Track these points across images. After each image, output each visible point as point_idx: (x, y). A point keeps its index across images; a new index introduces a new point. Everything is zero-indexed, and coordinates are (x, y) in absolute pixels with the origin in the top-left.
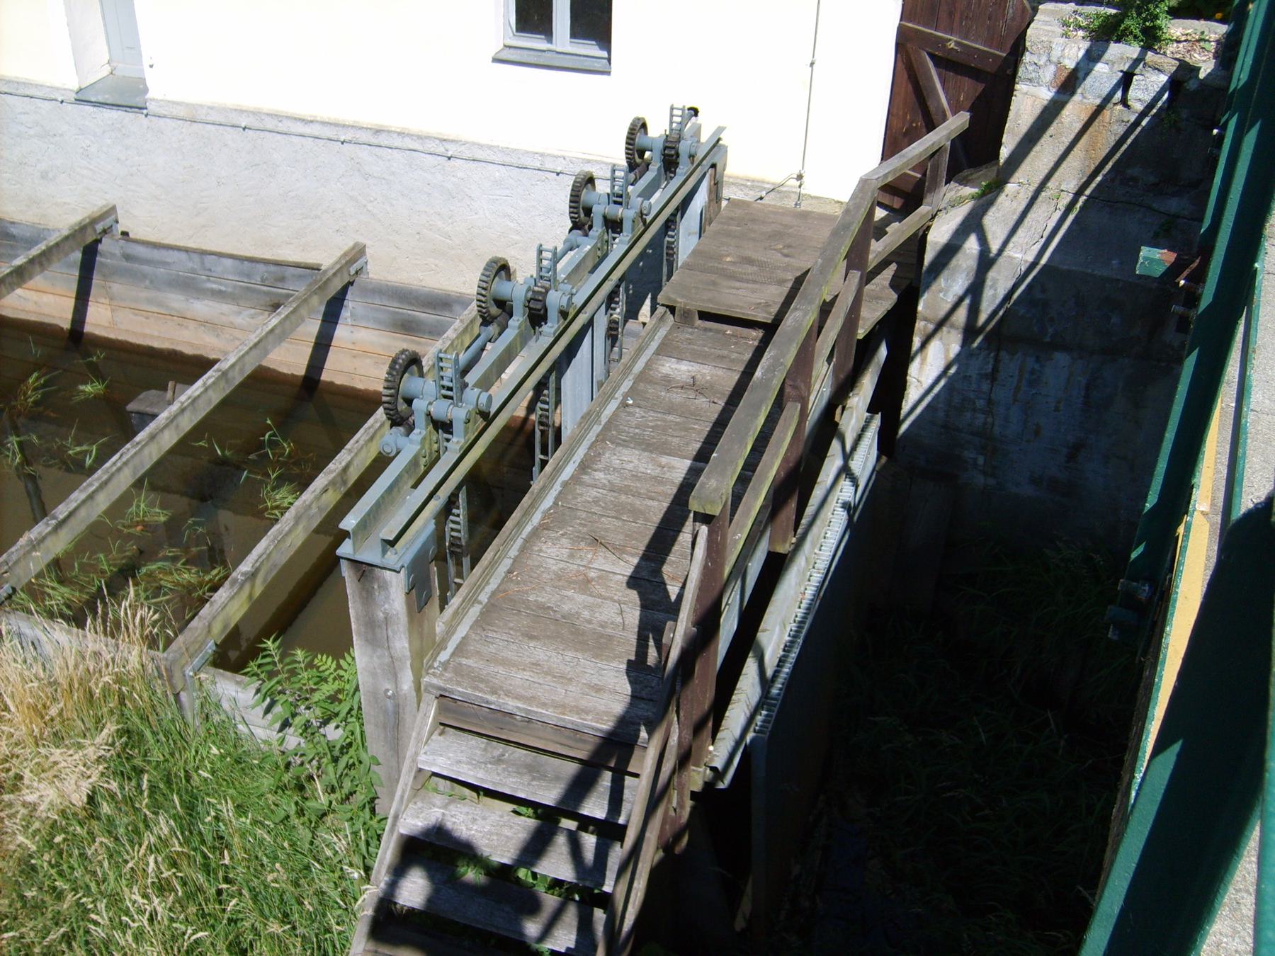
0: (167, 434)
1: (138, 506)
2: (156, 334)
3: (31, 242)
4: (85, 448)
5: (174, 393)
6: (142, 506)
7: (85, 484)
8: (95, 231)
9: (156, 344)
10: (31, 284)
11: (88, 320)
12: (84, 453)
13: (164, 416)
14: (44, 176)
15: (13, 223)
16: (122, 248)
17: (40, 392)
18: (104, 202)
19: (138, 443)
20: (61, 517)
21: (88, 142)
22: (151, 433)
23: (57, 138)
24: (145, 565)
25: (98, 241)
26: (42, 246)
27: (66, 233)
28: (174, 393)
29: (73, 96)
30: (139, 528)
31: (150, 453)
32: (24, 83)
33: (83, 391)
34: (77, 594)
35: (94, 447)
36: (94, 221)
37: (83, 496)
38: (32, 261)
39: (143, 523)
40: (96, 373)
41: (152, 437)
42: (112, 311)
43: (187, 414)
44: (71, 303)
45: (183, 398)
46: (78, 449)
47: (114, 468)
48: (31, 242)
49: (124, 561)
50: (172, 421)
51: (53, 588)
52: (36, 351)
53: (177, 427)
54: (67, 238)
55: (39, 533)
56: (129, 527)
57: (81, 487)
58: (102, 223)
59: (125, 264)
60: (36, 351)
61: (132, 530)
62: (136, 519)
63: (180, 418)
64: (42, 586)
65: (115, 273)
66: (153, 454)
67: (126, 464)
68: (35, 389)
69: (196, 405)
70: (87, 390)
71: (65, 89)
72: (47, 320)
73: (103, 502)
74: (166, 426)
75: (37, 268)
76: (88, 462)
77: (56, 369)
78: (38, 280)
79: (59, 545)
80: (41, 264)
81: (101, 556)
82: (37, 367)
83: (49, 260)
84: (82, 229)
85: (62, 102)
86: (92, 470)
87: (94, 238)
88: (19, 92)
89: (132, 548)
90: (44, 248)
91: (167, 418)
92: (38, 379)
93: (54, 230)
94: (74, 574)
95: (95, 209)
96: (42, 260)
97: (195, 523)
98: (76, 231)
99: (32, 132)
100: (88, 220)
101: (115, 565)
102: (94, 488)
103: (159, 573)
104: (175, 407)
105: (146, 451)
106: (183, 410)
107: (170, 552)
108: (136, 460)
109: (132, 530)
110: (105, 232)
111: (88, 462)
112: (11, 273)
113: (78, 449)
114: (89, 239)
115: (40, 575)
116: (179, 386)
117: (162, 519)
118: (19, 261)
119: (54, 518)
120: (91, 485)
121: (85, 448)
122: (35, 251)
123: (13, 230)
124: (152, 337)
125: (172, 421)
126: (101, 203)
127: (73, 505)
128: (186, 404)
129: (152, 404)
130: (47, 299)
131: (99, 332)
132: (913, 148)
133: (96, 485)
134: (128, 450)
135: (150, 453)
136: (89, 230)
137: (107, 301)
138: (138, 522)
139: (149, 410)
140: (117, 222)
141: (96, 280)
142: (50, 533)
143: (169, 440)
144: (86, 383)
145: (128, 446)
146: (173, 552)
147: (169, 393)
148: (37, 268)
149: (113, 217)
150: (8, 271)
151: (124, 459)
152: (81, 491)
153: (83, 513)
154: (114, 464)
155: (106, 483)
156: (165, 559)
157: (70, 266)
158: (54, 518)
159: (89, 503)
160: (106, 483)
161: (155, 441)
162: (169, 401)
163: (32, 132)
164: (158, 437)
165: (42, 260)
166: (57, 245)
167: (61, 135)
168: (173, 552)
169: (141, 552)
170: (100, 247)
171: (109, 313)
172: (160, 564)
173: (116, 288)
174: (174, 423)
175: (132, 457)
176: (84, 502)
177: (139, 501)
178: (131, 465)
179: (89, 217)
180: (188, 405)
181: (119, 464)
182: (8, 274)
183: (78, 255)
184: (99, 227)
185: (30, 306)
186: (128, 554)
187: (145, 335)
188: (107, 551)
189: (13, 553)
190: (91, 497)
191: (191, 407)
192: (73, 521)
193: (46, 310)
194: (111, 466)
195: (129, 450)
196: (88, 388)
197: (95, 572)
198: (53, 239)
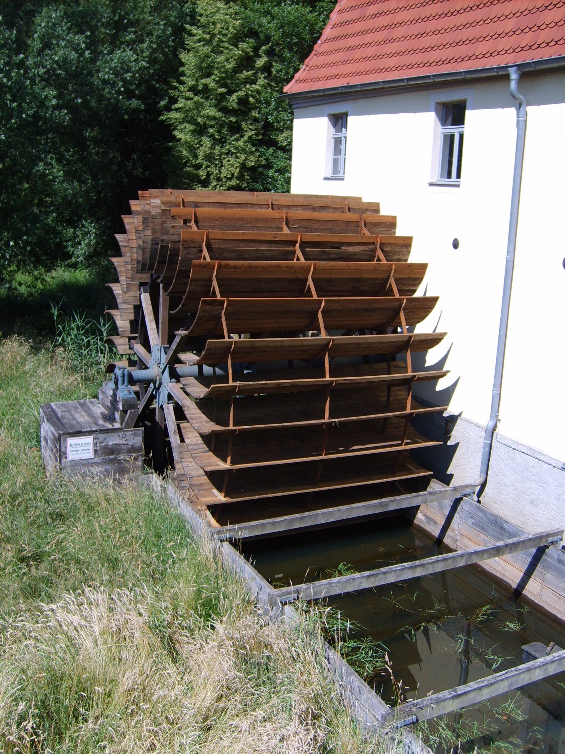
0: (538, 671)
1: (510, 705)
2: (561, 609)
3: (512, 535)
4: (495, 658)
5: (552, 649)
6: (512, 705)
7: (480, 680)
8: (547, 540)
9: (559, 616)
10: (504, 557)
11: (526, 587)
12: (494, 661)
13: (541, 660)
14: (532, 502)
15: (506, 522)
16: (559, 555)
17: (486, 617)
18: (559, 527)
19: (519, 670)
20: (459, 692)
21: (561, 492)
22: (528, 667)
23: (545, 485)
24: (498, 741)
25: (547, 547)
26: (515, 540)
27: (531, 536)
28: (552, 649)
29: (561, 465)
30: (505, 718)
31: (523, 679)
32: (538, 452)
33: (508, 626)
34: (454, 738)
35: (501, 660)
36: (548, 535)
37: (476, 686)
38: (506, 546)
39: (508, 715)
40: (520, 619)
41: (529, 670)
42: (542, 587)
43: (554, 665)
44: (521, 575)
45: (555, 655)
46: (492, 657)
47: (500, 678)
48: (512, 535)
49: (488, 733)
50: (544, 665)
51: (443, 729)
52: (494, 593)
53: (546, 669)
54: (530, 539)
55: (444, 696)
56: (500, 714)
57: (477, 681)
58: (553, 538)
59: (557, 564)
60: (494, 593)
61: (500, 717)
62: (505, 711)
63: (549, 666)
64: (439, 725)
65: (550, 567)
66: (525, 679)
67: (507, 678)
68: (484, 614)
69: (562, 661)
70: (510, 626)
71: (558, 461)
72: (505, 579)
73: (485, 694)
74: (539, 667)
75: (508, 551)
76: (494, 666)
77: (501, 608)
78: (508, 556)
79: (453, 706)
80: (511, 549)
81: (476, 723)
82: (491, 602)
83: (516, 548)
84: (540, 537)
85: (554, 467)
86: (496, 671)
87: (545, 544)
88: (534, 455)
89: (495, 727)
90: (516, 541)
91: (542, 663)
92: (488, 609)
93: (525, 533)
94: (458, 726)
95: (553, 529)
96: (512, 547)
97: (538, 731)
98: (537, 537)
99: (534, 478)
100: (545, 534)
101: (482, 732)
102: (484, 684)
103: (505, 750)
104: (549, 658)
105: (522, 676)
106: (552, 662)
107: (516, 740)
108: (514, 679)
109: (500, 717)
110: (552, 543)
111: (494, 666)
112: (494, 548)
113: (492, 657)
114: (543, 544)
115: (440, 718)
116: (556, 646)
117: (520, 719)
118: (500, 543)
119: (455, 691)
120: (483, 682)
121: (495, 658)
122: (510, 541)
123: (505, 526)
124: (558, 610)
125: (544, 665)
126: (557, 526)
127: (469, 689)
128: (555, 659)
129: (536, 651)
130: (510, 568)
131: (530, 596)
132: (317, 515)
133: (486, 683)
134: (512, 671)
135: (523, 679)
136: (544, 540)
137: (540, 581)
138: (506, 714)
139: (533, 653)
140: (561, 540)
141: (539, 567)
142: (449, 699)
143: (538, 675)
144: (511, 622)
145: (513, 669)
146: (518, 741)
147: (549, 649)
148: (508, 551)
149: (560, 537)
150: (492, 547)
151: (507, 675)
152: (476, 683)
153: (472, 695)
154: (501, 675)
155: (492, 684)
156: (511, 743)
157: (527, 555)
158: (455, 691)
159: (477, 691)
160: (492, 684)
161: (530, 672)
162: (546, 653)
163: (534, 478)
164: (532, 671)
165: (512, 547)
166: (523, 541)
167: (548, 484)
168: (518, 741)
169: (500, 732)
170: (547, 550)
171: (539, 588)
172: (507, 745)
173: (549, 576)
174: (545, 667)
175: (512, 676)
176: (475, 689)
177: (511, 702)
178: (510, 680)
179: (546, 532)
180: (557, 660)
181: (503, 677)
182: (491, 548)
183: (534, 551)
184: (550, 540)
185: (499, 569)
186: (492, 729)
187: (554, 608)
188: (481, 722)
189: (425, 700)
190: (480, 688)
191: (558, 662)
192: (464, 698)
193: (507, 574)
194: (499, 676)
195: (512, 671)
196: (511, 625)
197: (469, 731)
198: (522, 538)
